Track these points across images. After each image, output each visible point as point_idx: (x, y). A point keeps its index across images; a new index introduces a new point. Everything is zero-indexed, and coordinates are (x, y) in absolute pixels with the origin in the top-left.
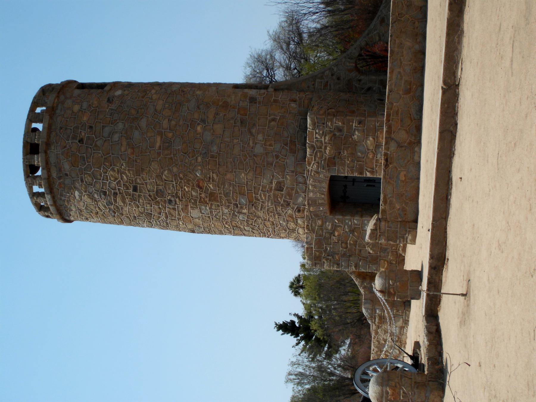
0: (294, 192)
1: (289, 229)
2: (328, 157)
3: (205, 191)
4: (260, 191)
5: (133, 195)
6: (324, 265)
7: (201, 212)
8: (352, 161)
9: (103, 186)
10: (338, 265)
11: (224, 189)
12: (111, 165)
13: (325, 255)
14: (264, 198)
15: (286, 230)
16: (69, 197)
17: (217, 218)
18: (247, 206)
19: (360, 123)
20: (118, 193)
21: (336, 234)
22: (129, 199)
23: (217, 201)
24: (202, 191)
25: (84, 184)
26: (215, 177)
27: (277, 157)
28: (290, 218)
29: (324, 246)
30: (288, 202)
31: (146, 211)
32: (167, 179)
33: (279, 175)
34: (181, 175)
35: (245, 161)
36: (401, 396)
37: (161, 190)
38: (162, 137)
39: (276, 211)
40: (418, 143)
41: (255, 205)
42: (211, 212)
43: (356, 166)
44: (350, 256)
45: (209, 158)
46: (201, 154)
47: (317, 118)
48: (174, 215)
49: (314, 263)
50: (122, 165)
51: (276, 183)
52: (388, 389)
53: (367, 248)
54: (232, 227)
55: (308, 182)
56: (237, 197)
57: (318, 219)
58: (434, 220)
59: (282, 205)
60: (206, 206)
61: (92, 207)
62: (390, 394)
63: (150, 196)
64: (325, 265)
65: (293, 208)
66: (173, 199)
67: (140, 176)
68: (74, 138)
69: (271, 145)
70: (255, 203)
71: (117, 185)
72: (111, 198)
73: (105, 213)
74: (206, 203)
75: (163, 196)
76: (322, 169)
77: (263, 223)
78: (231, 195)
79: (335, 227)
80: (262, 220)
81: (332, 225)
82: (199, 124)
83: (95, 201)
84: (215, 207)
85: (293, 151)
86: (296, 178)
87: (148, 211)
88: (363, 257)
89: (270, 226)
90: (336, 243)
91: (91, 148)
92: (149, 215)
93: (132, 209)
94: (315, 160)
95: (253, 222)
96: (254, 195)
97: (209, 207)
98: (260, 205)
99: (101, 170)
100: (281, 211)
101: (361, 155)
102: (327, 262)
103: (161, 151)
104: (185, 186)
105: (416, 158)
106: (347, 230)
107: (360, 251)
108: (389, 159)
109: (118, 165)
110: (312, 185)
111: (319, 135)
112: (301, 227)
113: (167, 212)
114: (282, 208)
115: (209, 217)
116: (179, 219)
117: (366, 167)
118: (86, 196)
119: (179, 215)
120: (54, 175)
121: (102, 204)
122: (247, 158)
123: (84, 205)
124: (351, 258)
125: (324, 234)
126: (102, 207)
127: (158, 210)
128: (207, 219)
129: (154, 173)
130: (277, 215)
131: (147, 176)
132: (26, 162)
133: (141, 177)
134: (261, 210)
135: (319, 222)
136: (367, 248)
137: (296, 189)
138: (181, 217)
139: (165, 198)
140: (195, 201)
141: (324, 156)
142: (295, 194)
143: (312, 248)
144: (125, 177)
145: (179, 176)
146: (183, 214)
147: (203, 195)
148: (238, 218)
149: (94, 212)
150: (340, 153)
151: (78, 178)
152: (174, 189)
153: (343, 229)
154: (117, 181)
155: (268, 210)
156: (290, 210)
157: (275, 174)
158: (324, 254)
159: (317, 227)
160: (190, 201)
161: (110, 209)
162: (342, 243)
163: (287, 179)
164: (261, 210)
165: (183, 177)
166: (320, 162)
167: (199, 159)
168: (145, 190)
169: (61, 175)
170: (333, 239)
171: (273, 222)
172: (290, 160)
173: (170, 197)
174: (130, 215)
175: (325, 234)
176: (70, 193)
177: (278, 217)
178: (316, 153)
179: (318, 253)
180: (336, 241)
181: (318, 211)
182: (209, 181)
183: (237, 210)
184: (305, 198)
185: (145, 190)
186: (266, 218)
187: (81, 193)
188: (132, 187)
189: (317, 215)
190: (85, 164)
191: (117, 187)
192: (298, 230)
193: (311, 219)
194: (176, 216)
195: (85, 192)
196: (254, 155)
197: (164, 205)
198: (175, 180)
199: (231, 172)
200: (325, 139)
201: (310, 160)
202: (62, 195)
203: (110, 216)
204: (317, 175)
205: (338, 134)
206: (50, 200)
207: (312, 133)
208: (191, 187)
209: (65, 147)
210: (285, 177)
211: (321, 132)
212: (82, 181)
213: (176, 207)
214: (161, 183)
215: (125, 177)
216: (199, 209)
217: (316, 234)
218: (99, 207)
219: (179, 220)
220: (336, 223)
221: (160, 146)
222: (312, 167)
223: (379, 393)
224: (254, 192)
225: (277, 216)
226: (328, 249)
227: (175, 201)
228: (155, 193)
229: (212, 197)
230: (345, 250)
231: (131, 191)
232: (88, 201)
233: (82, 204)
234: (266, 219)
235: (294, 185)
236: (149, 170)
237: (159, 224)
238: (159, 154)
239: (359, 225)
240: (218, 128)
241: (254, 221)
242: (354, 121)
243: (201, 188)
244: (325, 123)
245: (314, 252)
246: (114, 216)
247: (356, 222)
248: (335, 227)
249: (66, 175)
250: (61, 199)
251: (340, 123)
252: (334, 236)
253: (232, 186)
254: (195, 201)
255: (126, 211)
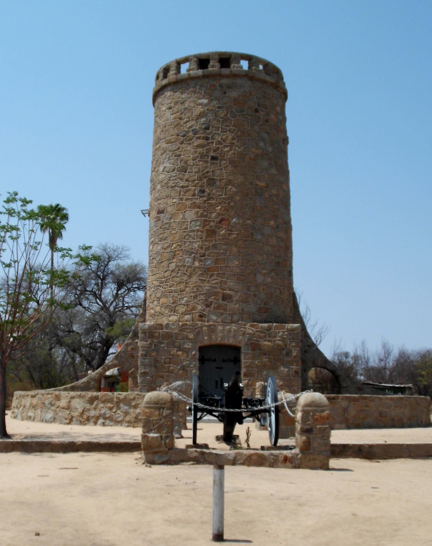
0: (222, 311)
1: (176, 306)
2: (260, 343)
3: (217, 226)
4: (220, 279)
5: (208, 156)
6: (144, 341)
7: (192, 221)
8: (257, 366)
9: (216, 127)
10: (145, 355)
11: (221, 244)
12: (238, 137)
13: (155, 342)
14: (213, 282)
15: (173, 303)
16: (199, 92)
17: (185, 236)
18: (203, 266)
19: (296, 372)
20: (209, 141)
21: (180, 353)
22: (203, 151)
23: (207, 237)
24: (217, 223)
25: (216, 109)
26: (233, 236)
27: (255, 295)
28: (191, 308)
29: (166, 342)
30: (211, 305)
31: (189, 167)
32: (227, 189)
33: (239, 297)
34: (232, 204)
35: (250, 265)
36: (320, 426)
37: (215, 183)
38: (264, 187)
39: (200, 294)
40: (349, 427)
41: (205, 273)
42: (193, 231)
43: (253, 370)
44: (156, 367)
45: (250, 231)
46: (254, 223)
47: (298, 333)
48: (186, 195)
49: (146, 331)
50: (239, 148)
51: (231, 295)
52: (327, 412)
53: (165, 383)
54: (174, 250)
55: (233, 325)
56: (213, 256)
57: (194, 335)
58: (408, 446)
59: (206, 300)
60: (200, 226)
61: (187, 115)
62: (322, 414)
63: (208, 172)
64: (144, 343)
65: (204, 310)
66: (206, 194)
67: (229, 164)
68: (259, 105)
69: (264, 290)
70: (207, 274)
71: (218, 141)
72: (201, 134)
73: (182, 127)
74: (204, 226)
75: (209, 184)
76: (249, 338)
77: (182, 281)
78: (214, 251)
79: (186, 351)
80: (186, 280)
81: (189, 349)
82: (275, 222)
83: (197, 119)
84: (200, 235)
85: (260, 310)
86: (237, 313)
87: (190, 169)
88: (155, 380)
89: (179, 288)
90: (170, 352)
91: (252, 119)
92: (184, 170)
93: (190, 153)
94: (257, 331)
95: (183, 271)
96: (216, 273)
97: (199, 229)
98: (205, 279)
99: (233, 126)
100: (199, 299)
101: (264, 374)
102: (148, 345)
103: (254, 186)
104: (222, 207)
105: (337, 425)
106: (184, 363)
107: (162, 377)
108: (335, 400)
109: (238, 144)
110: (230, 329)
111: (282, 335)
112: (179, 318)
113: (190, 187)
114: (203, 300)
115: (186, 228)
116: (181, 199)
117: (253, 379)
118: (202, 110)
119: (187, 199)
120: (224, 81)
121: (194, 125)
122: (253, 267)
123: (191, 107)
124: (153, 368)
125: (178, 341)
126: (189, 125)
127: (191, 179)
128: (184, 227)
129: (232, 177)
130: (195, 295)
131: (229, 171)
132: (235, 56)
133: (228, 164)
134: (199, 279)
135: (191, 336)
136: (165, 383)
137: (225, 313)
138: (184, 201)
139: (207, 187)
140: (206, 216)
141: (261, 340)
142: (220, 313)
143: (162, 329)
144: (226, 149)
145: (232, 201)
146: (188, 203)
147: (212, 224)
148: (188, 257)
149: (183, 116)
150: (265, 354)
151: (223, 104)
152: (217, 195)
153: (185, 360)
154: (222, 142)
155: (200, 286)
156: (202, 308)
157: (240, 293)
158: (156, 341)
159: (185, 333)
160: (205, 210)
161: (188, 132)
162: (170, 359)
163: (236, 304)
164: (199, 279)
165: (231, 205)
166: (255, 336)
167: (249, 222)
168: (214, 167)
169: (224, 88)
170: (173, 350)
171: (184, 291)
172: (252, 308)
173: (208, 191)
174: (182, 151)
175: (179, 342)
176: (205, 94)
177: (191, 296)
178: (264, 332)
179: (157, 335)
180: (171, 353)
181: (203, 335)
182: (228, 230)
183: (198, 256)
184: (216, 322)
185: (214, 167)
186: (190, 284)
187: (206, 105)
188: (217, 155)
189: (198, 333)
190: (237, 112)
191: (215, 141)
192: (175, 315)
193: (194, 328)
194: (185, 196)
195: (208, 110)
196: (255, 274)
197: (199, 185)
198: (228, 197)
199: (239, 252)
200: (279, 340)
201: (256, 327)
202: (201, 86)
203: (178, 131)
204: (241, 333)
205: (284, 352)
206: (196, 73)
207: (284, 328)
208: (221, 212)
209: (251, 94)
210: (237, 302)
211: (285, 337)
212: (219, 108)
213: (196, 197)
214: (223, 184)
215: (226, 149)
216: (197, 219)
217: (178, 333)
218: (189, 121)
219: (179, 200)
220: (192, 352)
221: (258, 185)
222: (249, 328)
223: (321, 403)
224: (220, 273)
225: (193, 294)
226: (163, 345)
227: (203, 197)
228: (212, 177)
229: (212, 233)
230: (162, 361)
231: (212, 154)
232: (196, 111)
233: (192, 105)
234: (188, 284)
235: (229, 311)
236: (235, 173)
237: (172, 179)
238: (251, 183)
239: (190, 375)
240: (273, 241)
241: (185, 272)
242: (297, 367)
243: (220, 222)
244: (294, 340)
245: (158, 331)
246: (178, 135)
247: (194, 371)
248: (186, 351)
249: (225, 93)
250: (196, 85)
251: (295, 354)
252: (177, 351)
253: (224, 252)
254: (206, 216)
255: (187, 147)
